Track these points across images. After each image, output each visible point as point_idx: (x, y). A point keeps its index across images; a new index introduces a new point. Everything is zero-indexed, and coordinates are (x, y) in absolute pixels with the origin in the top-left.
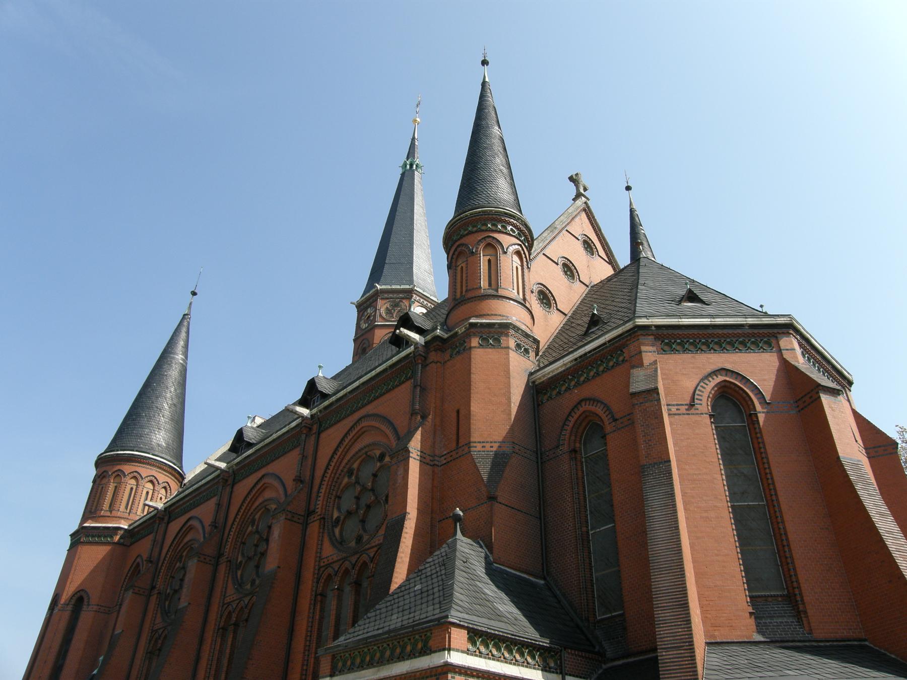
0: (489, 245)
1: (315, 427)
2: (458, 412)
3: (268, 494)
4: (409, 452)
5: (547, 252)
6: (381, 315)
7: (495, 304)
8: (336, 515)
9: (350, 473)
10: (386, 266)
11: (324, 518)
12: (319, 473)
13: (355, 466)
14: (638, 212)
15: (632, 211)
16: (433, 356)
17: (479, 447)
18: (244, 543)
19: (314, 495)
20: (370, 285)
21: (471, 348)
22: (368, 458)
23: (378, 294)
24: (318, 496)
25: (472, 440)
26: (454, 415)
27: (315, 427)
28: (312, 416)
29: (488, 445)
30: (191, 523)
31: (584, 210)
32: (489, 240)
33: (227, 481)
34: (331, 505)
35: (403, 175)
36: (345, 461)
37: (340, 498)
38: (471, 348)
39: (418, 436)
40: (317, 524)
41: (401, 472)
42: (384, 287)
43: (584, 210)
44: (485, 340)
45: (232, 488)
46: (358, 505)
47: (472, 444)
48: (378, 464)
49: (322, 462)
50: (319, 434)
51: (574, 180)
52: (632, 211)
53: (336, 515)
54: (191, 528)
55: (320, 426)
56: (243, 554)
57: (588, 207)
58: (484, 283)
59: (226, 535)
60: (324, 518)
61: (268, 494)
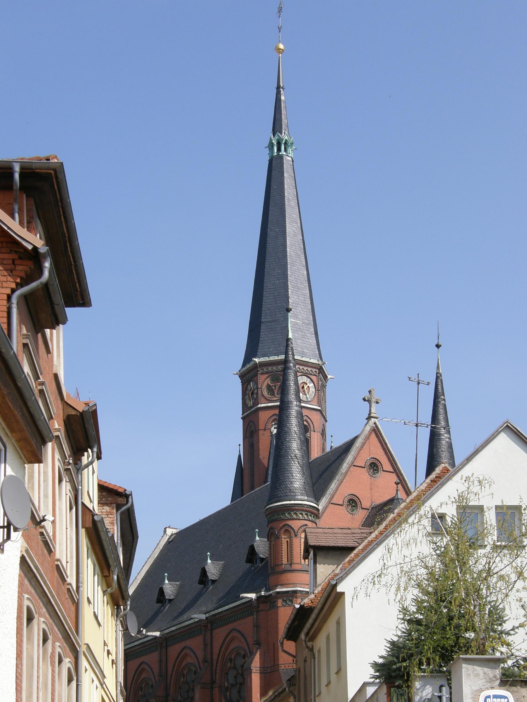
0: (287, 530)
1: (209, 625)
2: (274, 644)
3: (189, 660)
4: (251, 670)
5: (334, 501)
6: (263, 395)
7: (290, 577)
8: (226, 684)
9: (231, 660)
10: (263, 327)
11: (220, 686)
12: (215, 657)
13: (233, 657)
14: (444, 378)
15: (438, 377)
16: (262, 606)
17: (282, 667)
18: (180, 688)
19: (214, 672)
20: (247, 359)
21: (278, 607)
22: (238, 654)
23: (256, 366)
24: (216, 673)
25: (280, 663)
26: (272, 645)
27: (209, 625)
28: (207, 618)
29: (287, 665)
30: (142, 666)
31: (374, 430)
32: (286, 527)
33: (162, 643)
34: (223, 678)
35: (271, 162)
36: (227, 654)
37: (227, 674)
38: (278, 607)
39: (258, 652)
40: (217, 689)
41: (249, 680)
42: (262, 359)
43: (374, 430)
44: (284, 601)
45: (166, 649)
46: (236, 681)
47: (280, 666)
48: (243, 660)
49: (216, 651)
50: (212, 631)
51: (370, 392)
52: (438, 377)
53: (226, 684)
54: (143, 670)
55: (212, 625)
56: (181, 696)
57: (377, 427)
58: (285, 561)
59: (169, 681)
60: (220, 686)
61: (189, 660)
